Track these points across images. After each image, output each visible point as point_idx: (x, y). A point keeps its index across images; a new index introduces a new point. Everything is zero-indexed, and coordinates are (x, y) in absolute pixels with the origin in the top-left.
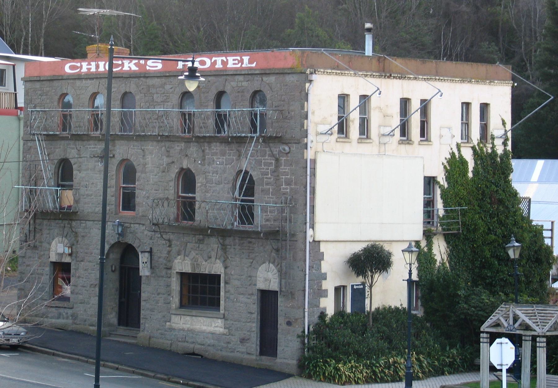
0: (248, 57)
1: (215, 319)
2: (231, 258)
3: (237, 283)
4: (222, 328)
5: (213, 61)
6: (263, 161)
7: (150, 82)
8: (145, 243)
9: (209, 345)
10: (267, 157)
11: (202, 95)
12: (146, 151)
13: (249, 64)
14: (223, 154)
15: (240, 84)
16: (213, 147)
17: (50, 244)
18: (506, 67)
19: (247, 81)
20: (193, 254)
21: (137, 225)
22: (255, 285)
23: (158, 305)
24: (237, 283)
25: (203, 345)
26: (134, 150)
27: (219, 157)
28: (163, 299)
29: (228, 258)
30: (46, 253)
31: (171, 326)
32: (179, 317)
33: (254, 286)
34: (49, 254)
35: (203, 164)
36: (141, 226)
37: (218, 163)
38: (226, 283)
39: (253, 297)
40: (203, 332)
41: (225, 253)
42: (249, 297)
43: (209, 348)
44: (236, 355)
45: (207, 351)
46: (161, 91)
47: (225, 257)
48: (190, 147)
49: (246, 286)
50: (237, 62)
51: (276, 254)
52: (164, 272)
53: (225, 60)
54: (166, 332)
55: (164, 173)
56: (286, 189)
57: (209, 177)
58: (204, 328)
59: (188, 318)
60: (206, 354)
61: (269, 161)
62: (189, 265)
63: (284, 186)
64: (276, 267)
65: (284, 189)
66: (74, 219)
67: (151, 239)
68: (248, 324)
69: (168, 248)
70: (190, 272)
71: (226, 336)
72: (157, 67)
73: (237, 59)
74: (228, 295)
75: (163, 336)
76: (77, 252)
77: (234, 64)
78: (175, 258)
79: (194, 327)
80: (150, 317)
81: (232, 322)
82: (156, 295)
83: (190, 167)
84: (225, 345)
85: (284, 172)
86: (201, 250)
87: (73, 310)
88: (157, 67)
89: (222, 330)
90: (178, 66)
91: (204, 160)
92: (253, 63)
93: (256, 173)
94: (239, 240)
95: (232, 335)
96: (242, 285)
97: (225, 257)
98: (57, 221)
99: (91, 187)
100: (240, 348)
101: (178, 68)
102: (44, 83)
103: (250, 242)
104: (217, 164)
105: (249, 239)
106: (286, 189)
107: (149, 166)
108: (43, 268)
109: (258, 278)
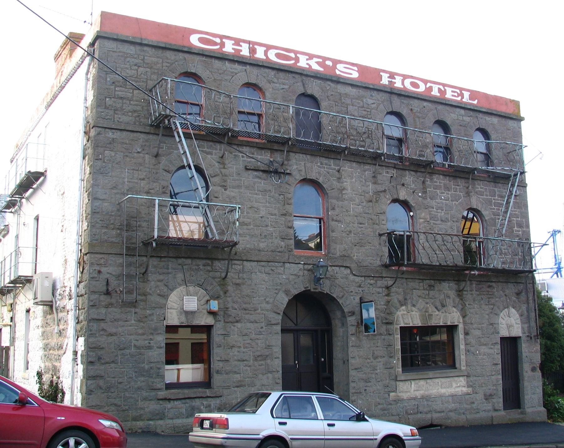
0: (433, 93)
1: (456, 378)
2: (469, 305)
3: (478, 333)
4: (465, 386)
5: (428, 86)
6: (493, 201)
7: (341, 89)
8: (352, 292)
9: (451, 411)
10: (497, 198)
11: (417, 119)
12: (343, 173)
13: (470, 100)
14: (448, 189)
15: (461, 118)
16: (435, 180)
17: (165, 297)
18: (198, 177)
19: (469, 117)
20: (421, 304)
21: (337, 268)
22: (498, 333)
23: (376, 372)
24: (478, 333)
25: (443, 412)
26: (323, 170)
27: (443, 191)
28: (381, 363)
29: (465, 305)
30: (158, 311)
31: (398, 396)
32: (408, 383)
33: (496, 334)
34: (164, 314)
35: (425, 198)
36: (343, 269)
37: (443, 197)
38: (466, 334)
39: (496, 347)
40: (441, 396)
41: (462, 299)
42: (492, 347)
43: (451, 413)
44: (483, 415)
45: (449, 418)
46: (359, 103)
47: (463, 304)
48: (405, 176)
49: (488, 336)
50: (456, 94)
51: (517, 298)
52: (383, 329)
53: (443, 89)
54: (390, 406)
55: (370, 204)
56: (519, 231)
57: (433, 213)
58: (443, 391)
59: (422, 382)
60: (449, 422)
61: (499, 201)
62: (418, 318)
63: (516, 228)
64: (518, 311)
65: (516, 231)
66: (220, 257)
67: (360, 286)
68: (493, 377)
69: (386, 298)
70: (420, 325)
71: (470, 396)
72: (351, 74)
73: (457, 93)
74: (469, 347)
75: (386, 412)
76: (227, 308)
77: (453, 96)
78: (397, 309)
79: (431, 392)
80: (365, 390)
81: (475, 378)
82: (372, 359)
83: (408, 199)
84: (469, 407)
85: (515, 214)
86: (431, 298)
87: (222, 399)
88: (351, 74)
89: (465, 390)
90: (382, 81)
91: (425, 192)
92: (474, 100)
93: (487, 212)
94: (476, 284)
95: (476, 393)
96: (483, 334)
97: (463, 304)
98: (180, 261)
99: (248, 213)
100: (486, 406)
101: (381, 82)
102: (146, 48)
103: (490, 287)
104: (441, 199)
105: (489, 283)
106: (519, 231)
107: (349, 191)
108: (152, 337)
109: (500, 325)
